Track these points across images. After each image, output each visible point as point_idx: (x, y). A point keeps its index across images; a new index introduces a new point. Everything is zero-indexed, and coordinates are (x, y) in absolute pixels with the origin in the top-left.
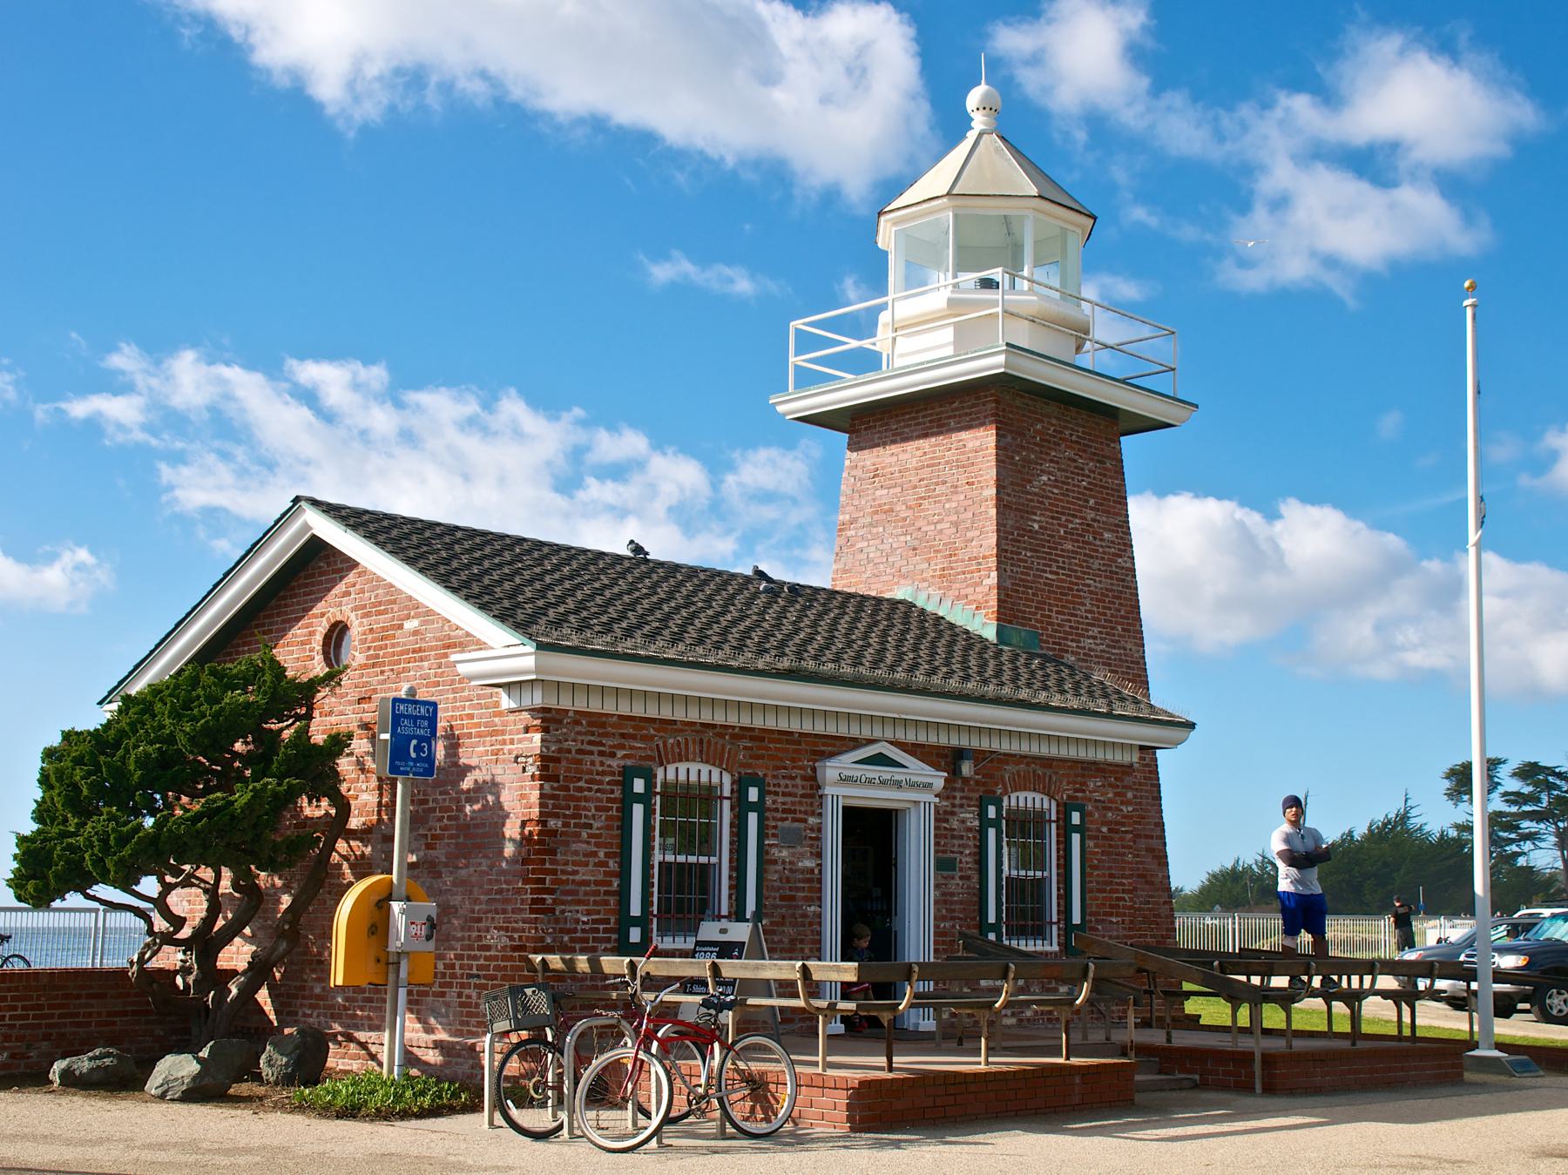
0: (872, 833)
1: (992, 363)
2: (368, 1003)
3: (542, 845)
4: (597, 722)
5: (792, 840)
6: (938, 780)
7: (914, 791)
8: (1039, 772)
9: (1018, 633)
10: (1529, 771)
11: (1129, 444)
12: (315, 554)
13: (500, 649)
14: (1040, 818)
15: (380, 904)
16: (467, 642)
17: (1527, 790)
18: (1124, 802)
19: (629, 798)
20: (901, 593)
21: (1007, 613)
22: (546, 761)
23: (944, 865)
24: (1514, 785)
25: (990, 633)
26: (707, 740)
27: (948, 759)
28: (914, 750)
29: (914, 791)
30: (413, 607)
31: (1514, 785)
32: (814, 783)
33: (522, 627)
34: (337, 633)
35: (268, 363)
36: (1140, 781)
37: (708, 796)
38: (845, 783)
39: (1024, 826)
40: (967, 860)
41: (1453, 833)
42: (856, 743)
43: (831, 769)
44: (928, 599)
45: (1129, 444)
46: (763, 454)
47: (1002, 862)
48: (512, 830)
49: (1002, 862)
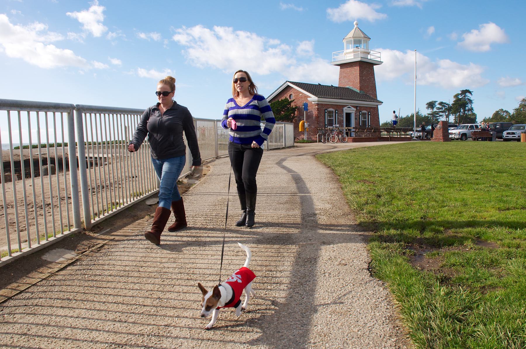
0: (348, 115)
1: (359, 59)
2: (302, 133)
3: (318, 117)
4: (322, 104)
5: (341, 116)
6: (355, 109)
7: (352, 111)
8: (366, 108)
9: (362, 92)
10: (441, 103)
11: (375, 66)
12: (288, 86)
13: (313, 98)
14: (366, 113)
15: (304, 123)
16: (310, 97)
17: (440, 107)
18: (374, 112)
19: (325, 112)
20: (347, 87)
21: (361, 89)
22: (318, 109)
23: (356, 119)
24: (438, 106)
25: (359, 92)
26: (332, 106)
27: (356, 107)
28: (352, 106)
29: (352, 111)
30: (301, 93)
31: (438, 106)
32: (343, 110)
33: (315, 95)
34: (291, 95)
35: (211, 28)
36: (376, 109)
37: (332, 112)
38: (346, 110)
39: (364, 114)
40: (358, 118)
41: (427, 115)
42: (347, 106)
43: (345, 108)
44: (351, 87)
45: (375, 66)
46: (304, 42)
47: (362, 119)
48: (314, 116)
49: (362, 119)
